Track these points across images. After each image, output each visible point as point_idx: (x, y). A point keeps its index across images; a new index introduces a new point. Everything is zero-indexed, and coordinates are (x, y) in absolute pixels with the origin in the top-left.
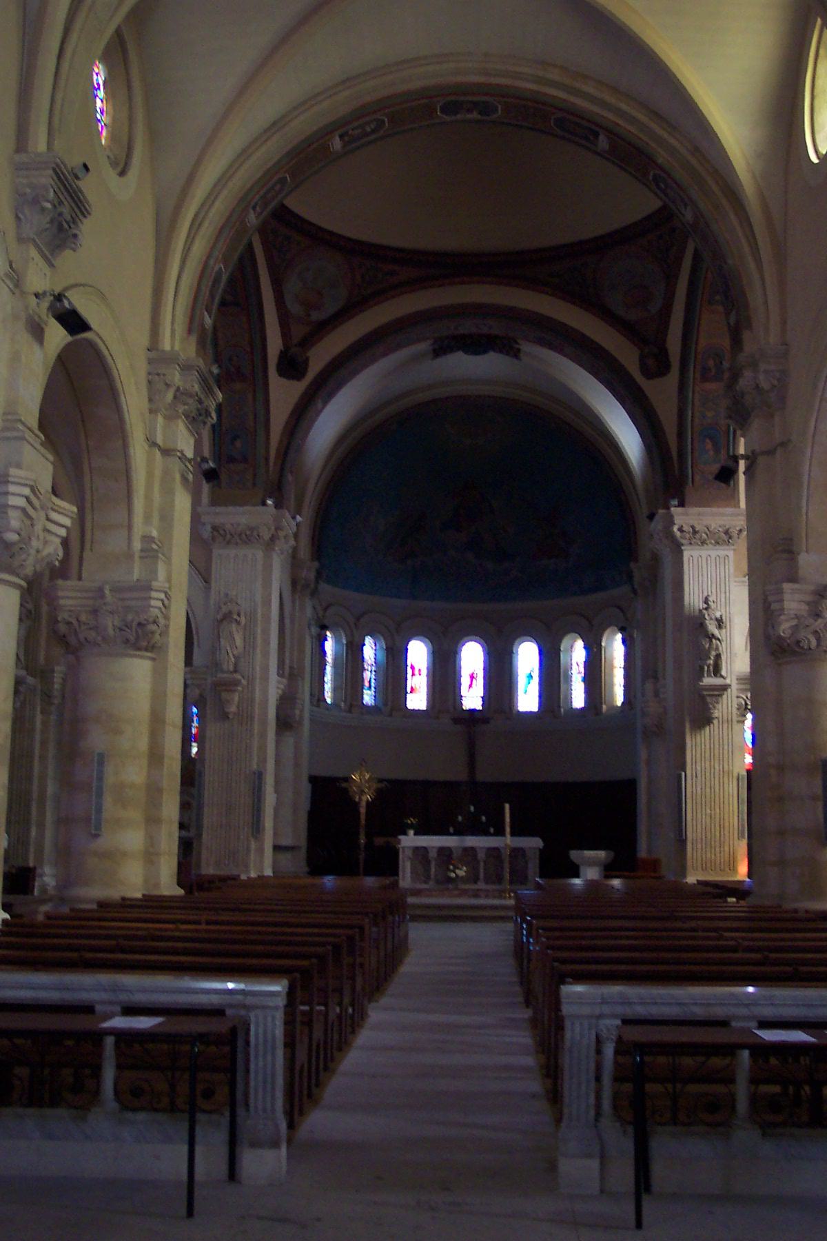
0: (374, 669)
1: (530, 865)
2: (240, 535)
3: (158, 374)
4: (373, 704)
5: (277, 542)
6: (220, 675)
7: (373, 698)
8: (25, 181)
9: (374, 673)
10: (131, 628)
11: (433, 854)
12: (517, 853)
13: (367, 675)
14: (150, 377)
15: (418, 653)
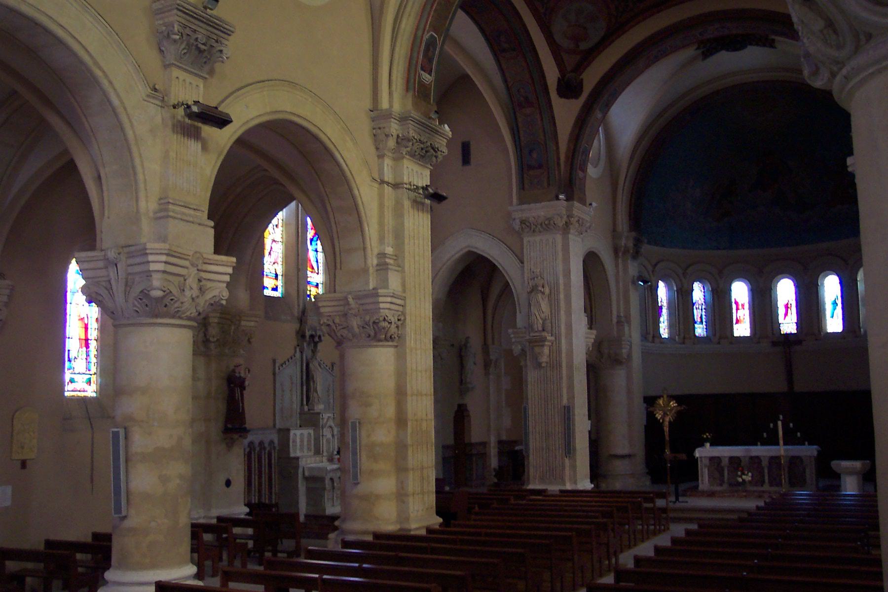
0: (703, 307)
1: (808, 471)
2: (541, 225)
3: (380, 128)
4: (705, 335)
5: (571, 226)
6: (532, 334)
7: (705, 330)
8: (161, 22)
9: (704, 310)
10: (369, 326)
11: (725, 462)
12: (794, 461)
13: (697, 314)
14: (374, 131)
15: (740, 291)
